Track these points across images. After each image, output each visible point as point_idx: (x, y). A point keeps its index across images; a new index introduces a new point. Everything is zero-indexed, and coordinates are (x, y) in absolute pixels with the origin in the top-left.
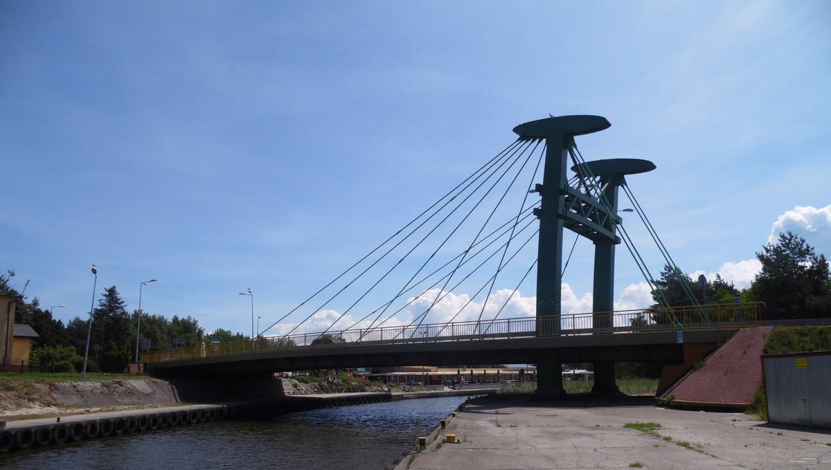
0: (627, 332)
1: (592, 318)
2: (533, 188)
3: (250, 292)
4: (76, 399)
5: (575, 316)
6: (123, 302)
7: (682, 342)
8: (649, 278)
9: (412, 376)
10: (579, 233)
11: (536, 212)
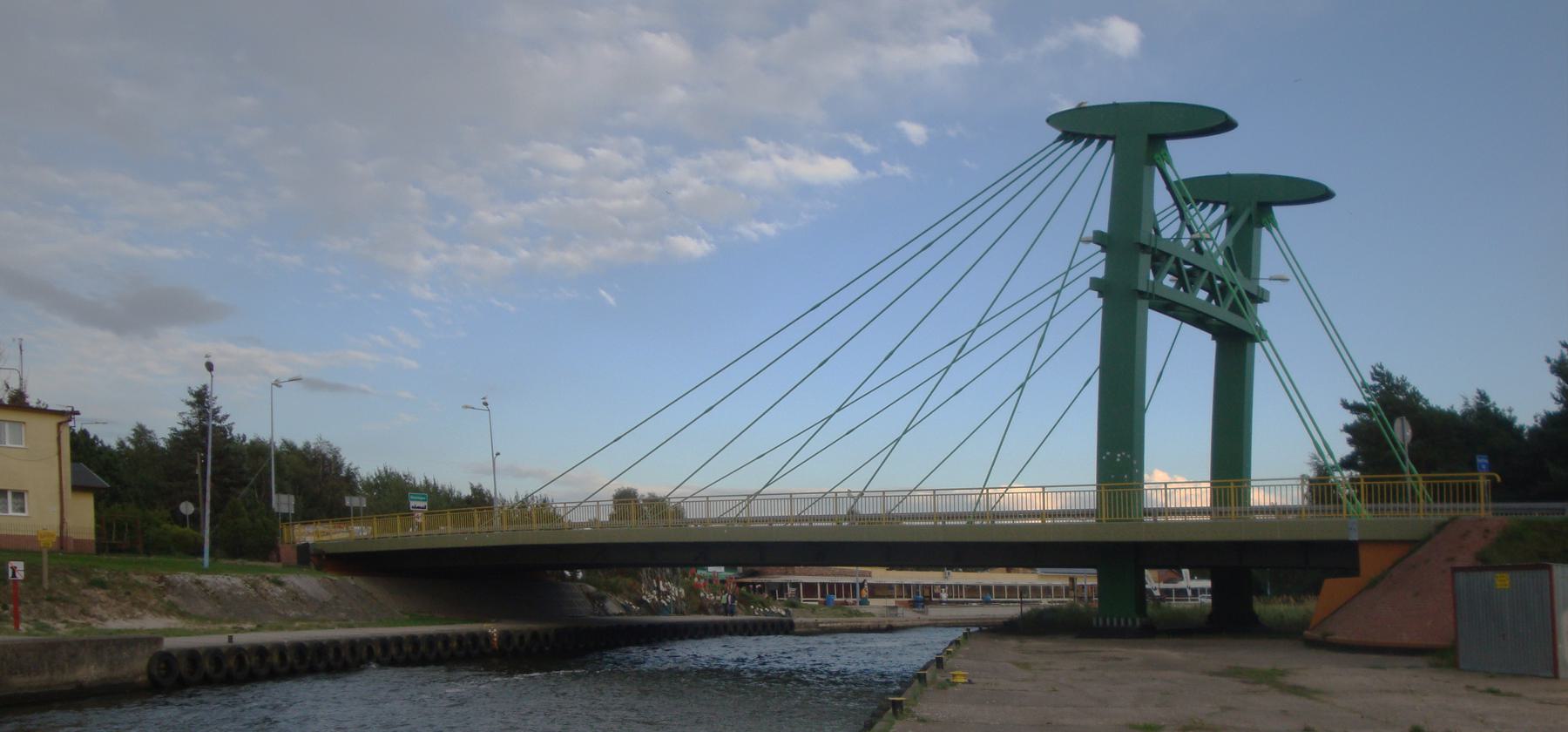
1: (1209, 489)
2: (1089, 234)
3: (486, 404)
4: (207, 608)
6: (227, 416)
7: (1356, 539)
8: (1359, 380)
9: (831, 585)
10: (1183, 320)
11: (1096, 285)
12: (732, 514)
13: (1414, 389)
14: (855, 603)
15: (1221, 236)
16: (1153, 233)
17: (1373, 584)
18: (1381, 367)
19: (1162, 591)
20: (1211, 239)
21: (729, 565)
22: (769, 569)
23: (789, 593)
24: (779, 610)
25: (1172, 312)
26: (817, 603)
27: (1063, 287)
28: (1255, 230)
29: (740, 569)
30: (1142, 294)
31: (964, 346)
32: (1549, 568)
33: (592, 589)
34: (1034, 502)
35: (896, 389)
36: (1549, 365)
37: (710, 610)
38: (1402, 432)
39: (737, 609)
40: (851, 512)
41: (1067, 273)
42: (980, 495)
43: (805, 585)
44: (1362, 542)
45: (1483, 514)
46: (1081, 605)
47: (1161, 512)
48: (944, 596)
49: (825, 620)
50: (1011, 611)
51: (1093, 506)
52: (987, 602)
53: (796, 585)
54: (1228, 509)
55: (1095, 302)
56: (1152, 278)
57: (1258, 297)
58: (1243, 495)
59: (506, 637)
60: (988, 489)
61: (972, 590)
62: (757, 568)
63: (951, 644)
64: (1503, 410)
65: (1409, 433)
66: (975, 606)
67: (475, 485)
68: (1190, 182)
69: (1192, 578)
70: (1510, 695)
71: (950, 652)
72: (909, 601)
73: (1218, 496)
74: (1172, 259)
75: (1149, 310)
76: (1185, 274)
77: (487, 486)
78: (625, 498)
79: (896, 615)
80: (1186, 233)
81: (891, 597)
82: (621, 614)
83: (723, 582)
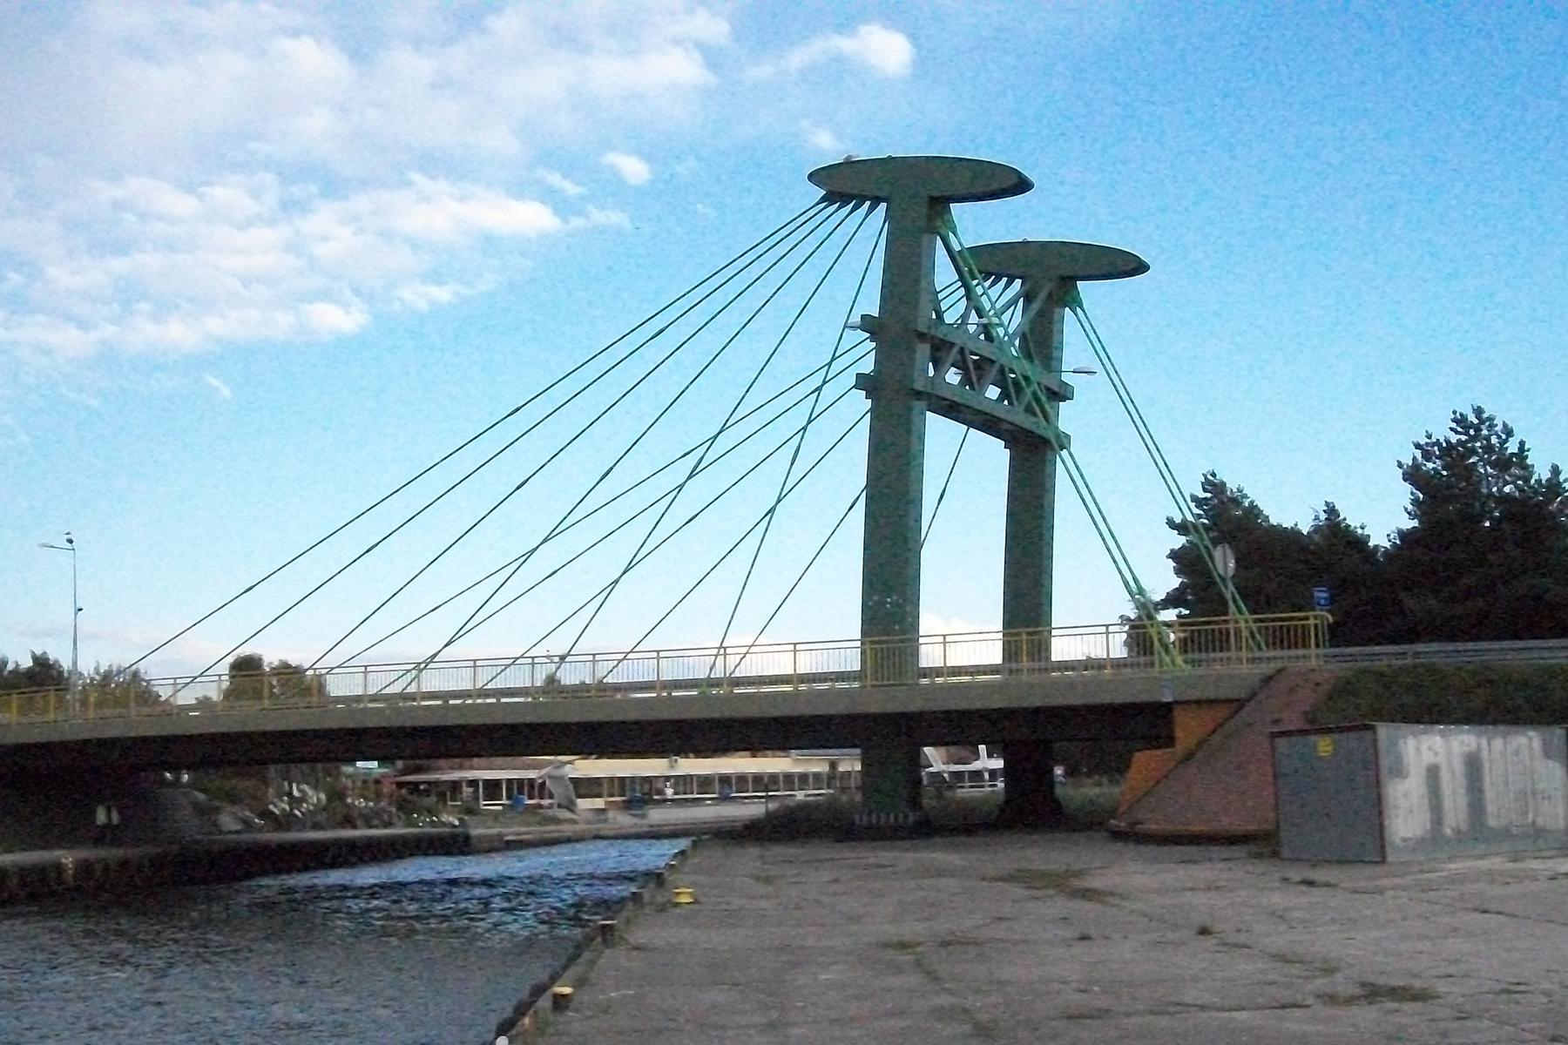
0: (522, 700)
2: (856, 319)
5: (948, 639)
7: (1170, 699)
9: (520, 782)
10: (970, 424)
11: (863, 382)
12: (396, 689)
13: (1252, 502)
14: (550, 807)
15: (1015, 319)
16: (934, 316)
17: (1189, 756)
18: (1214, 475)
19: (952, 774)
20: (1001, 325)
21: (383, 760)
22: (442, 762)
23: (464, 794)
24: (451, 819)
25: (954, 414)
26: (500, 808)
27: (825, 382)
28: (1057, 310)
29: (400, 764)
30: (918, 395)
31: (702, 458)
32: (1372, 728)
33: (201, 797)
34: (781, 665)
35: (607, 519)
36: (1401, 471)
37: (359, 823)
38: (1224, 562)
39: (395, 820)
40: (551, 680)
41: (830, 364)
42: (716, 656)
43: (486, 782)
44: (1177, 702)
45: (1314, 663)
46: (844, 798)
47: (938, 672)
48: (669, 792)
49: (511, 831)
50: (751, 809)
51: (856, 666)
52: (725, 799)
53: (473, 783)
54: (1020, 666)
55: (861, 403)
56: (931, 372)
57: (1060, 394)
58: (1041, 648)
59: (85, 868)
60: (725, 648)
61: (705, 782)
62: (425, 762)
63: (675, 856)
64: (1356, 528)
65: (1232, 564)
66: (709, 805)
67: (38, 653)
68: (975, 251)
69: (990, 755)
70: (1327, 885)
71: (673, 865)
72: (624, 801)
73: (1010, 652)
74: (955, 350)
75: (928, 413)
76: (971, 366)
77: (61, 655)
78: (246, 667)
79: (606, 820)
80: (973, 318)
81: (599, 796)
82: (237, 832)
83: (377, 782)
